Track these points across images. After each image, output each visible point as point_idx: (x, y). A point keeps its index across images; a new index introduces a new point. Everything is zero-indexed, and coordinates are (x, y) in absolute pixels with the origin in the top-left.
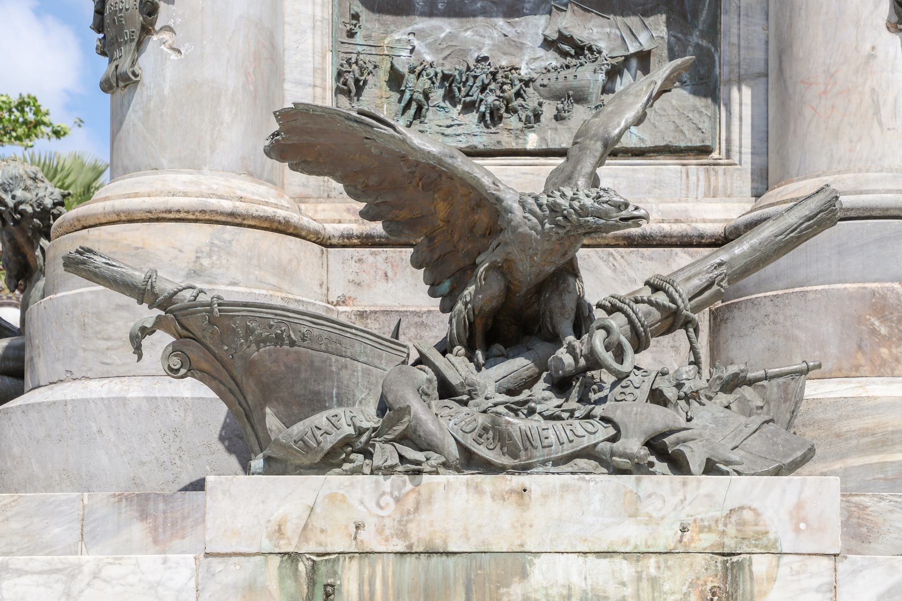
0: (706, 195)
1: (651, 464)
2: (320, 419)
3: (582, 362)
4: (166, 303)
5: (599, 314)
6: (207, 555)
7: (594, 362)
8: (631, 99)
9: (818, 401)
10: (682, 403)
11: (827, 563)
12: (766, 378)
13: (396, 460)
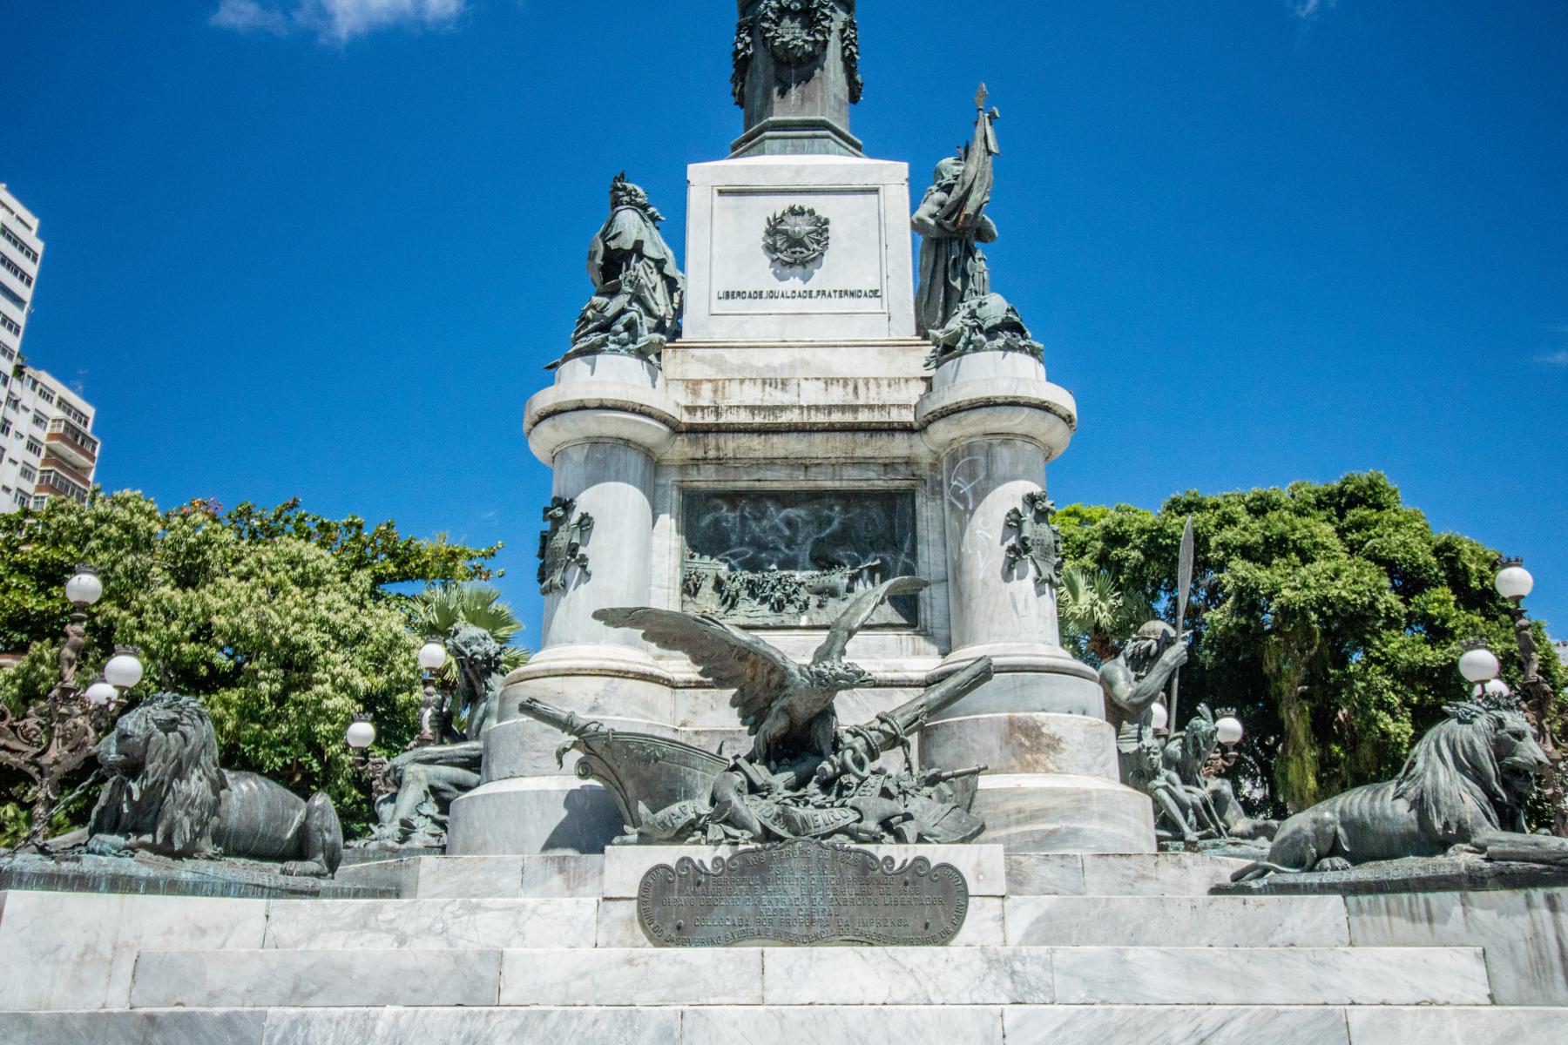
0: (913, 654)
1: (883, 837)
2: (675, 808)
3: (838, 770)
4: (581, 732)
5: (848, 739)
6: (605, 899)
7: (845, 770)
8: (864, 606)
10: (901, 796)
11: (998, 901)
12: (953, 776)
13: (722, 836)
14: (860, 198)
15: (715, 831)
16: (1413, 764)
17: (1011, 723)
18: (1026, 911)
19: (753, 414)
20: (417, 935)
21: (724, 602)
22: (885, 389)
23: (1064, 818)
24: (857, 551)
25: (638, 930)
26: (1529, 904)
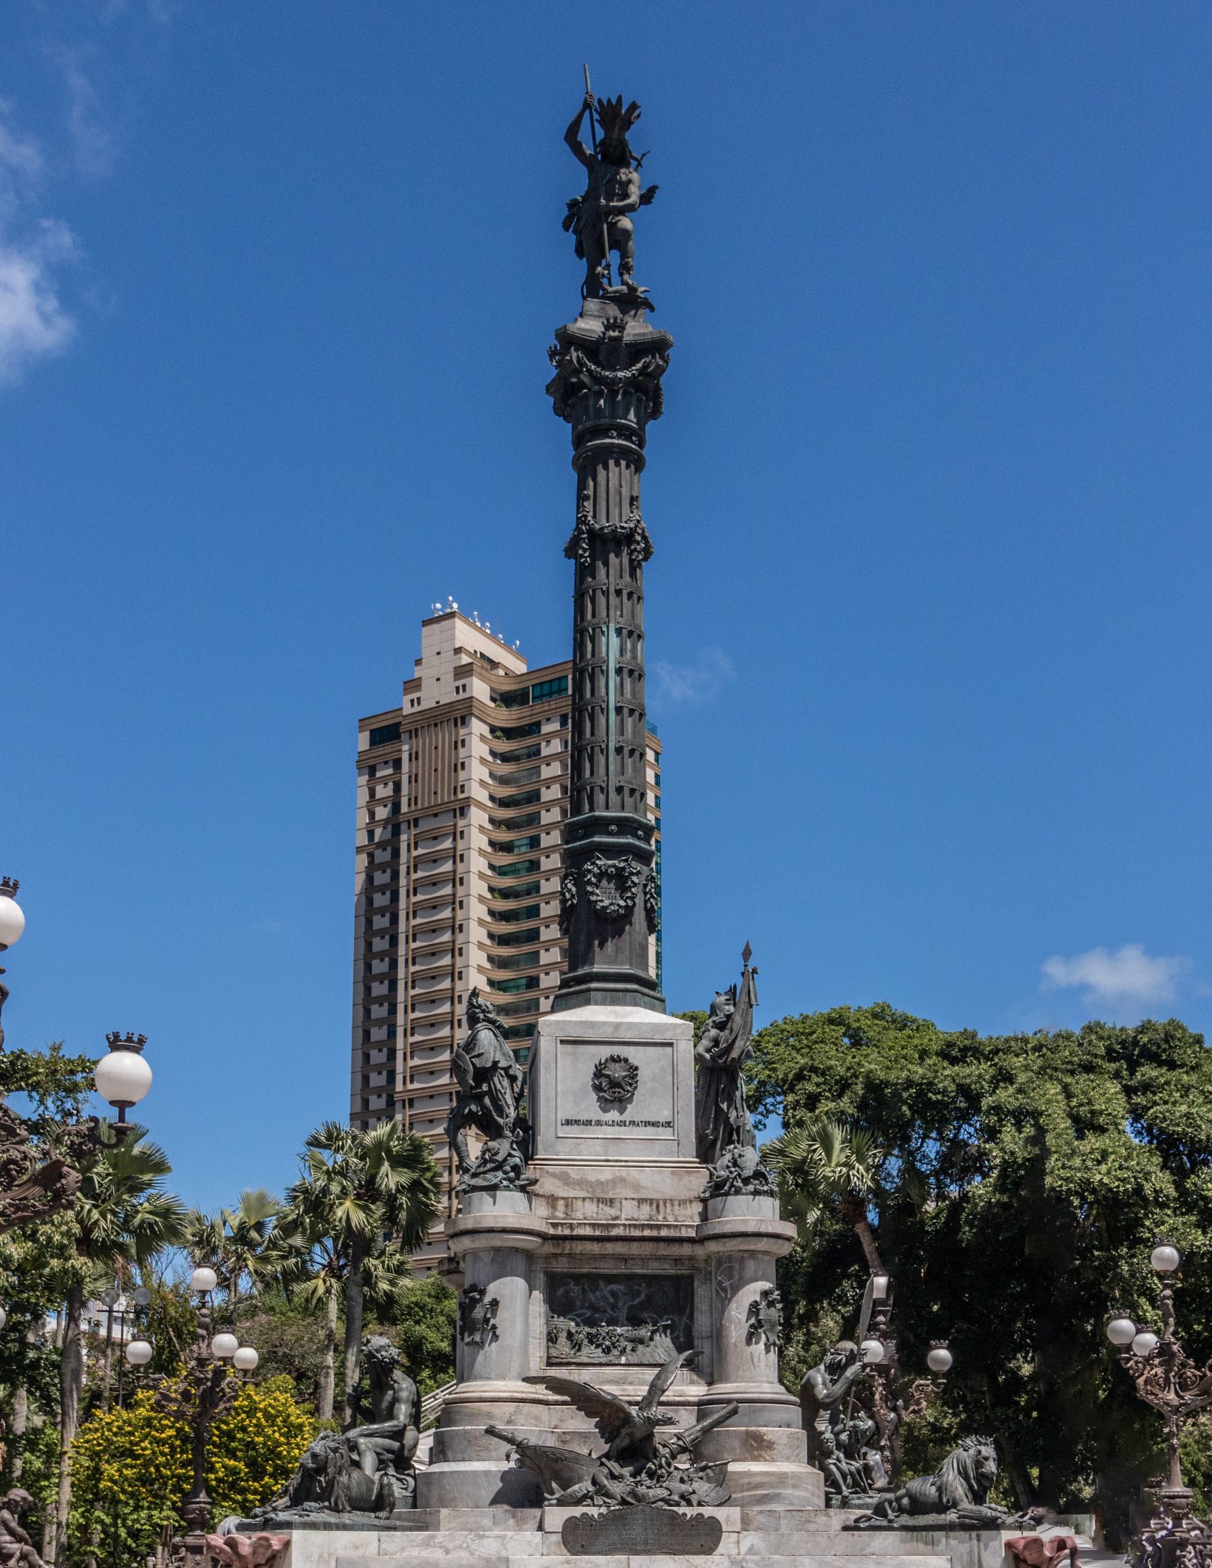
2: (576, 1487)
7: (661, 1467)
9: (734, 1473)
14: (660, 1049)
15: (599, 1500)
16: (942, 1469)
17: (747, 1433)
18: (751, 1539)
19: (594, 1230)
20: (455, 1549)
21: (574, 1347)
22: (677, 1207)
23: (772, 1487)
24: (656, 1313)
25: (563, 1547)
26: (970, 1539)
